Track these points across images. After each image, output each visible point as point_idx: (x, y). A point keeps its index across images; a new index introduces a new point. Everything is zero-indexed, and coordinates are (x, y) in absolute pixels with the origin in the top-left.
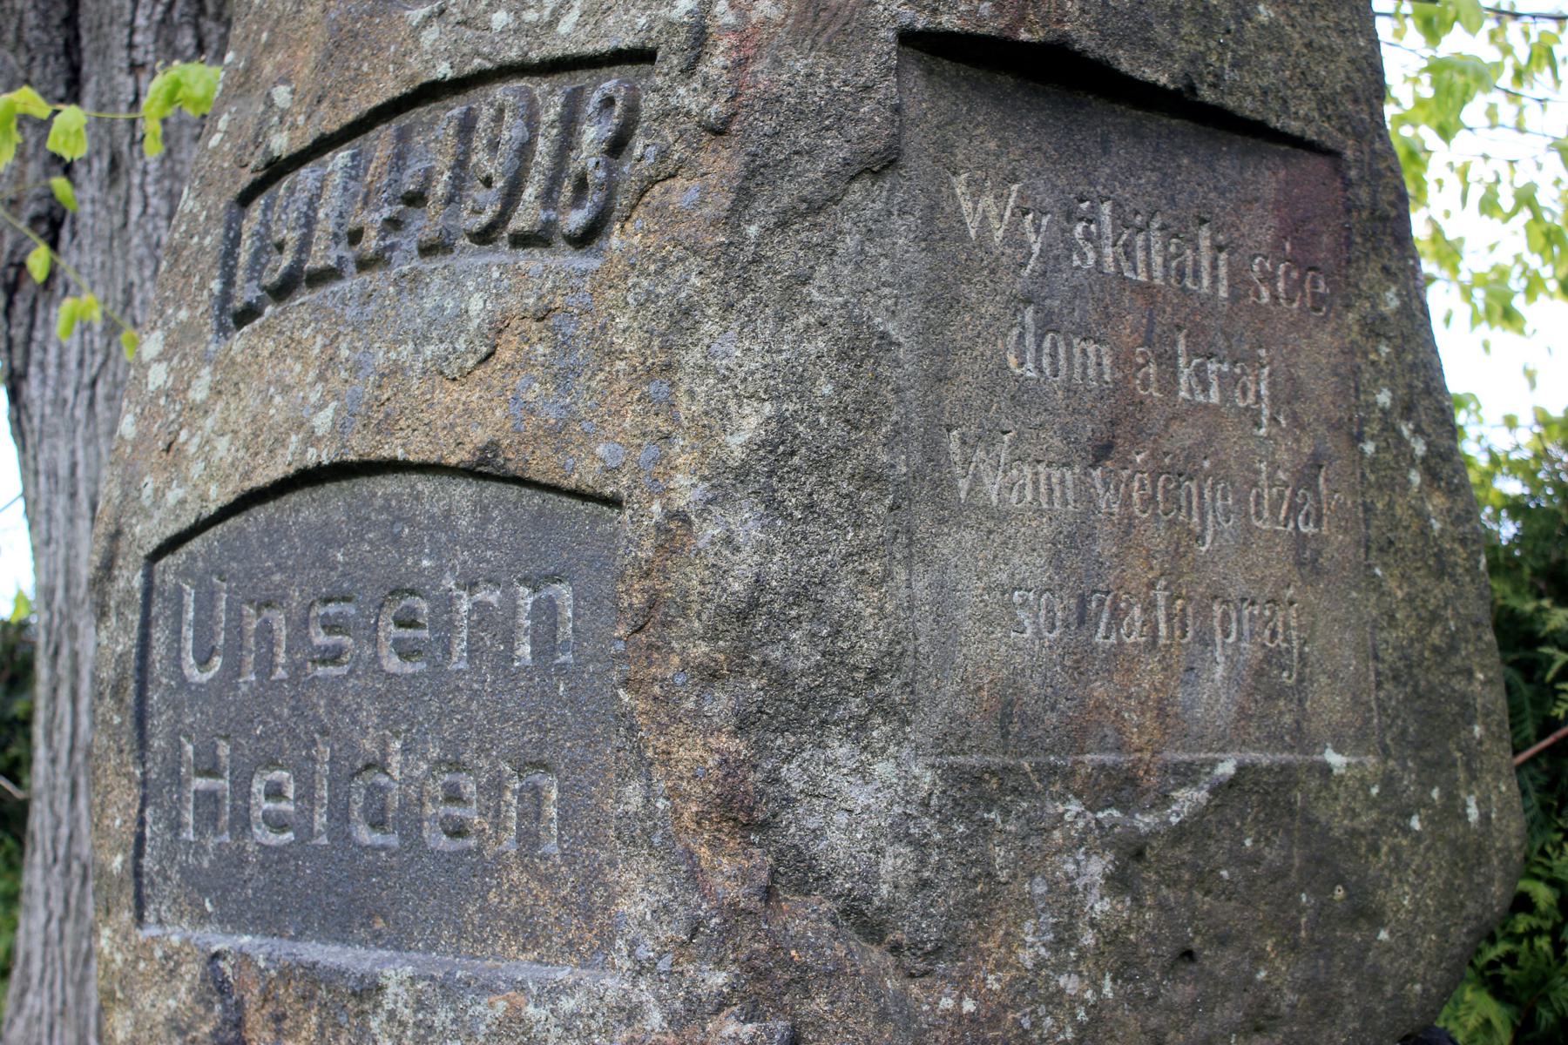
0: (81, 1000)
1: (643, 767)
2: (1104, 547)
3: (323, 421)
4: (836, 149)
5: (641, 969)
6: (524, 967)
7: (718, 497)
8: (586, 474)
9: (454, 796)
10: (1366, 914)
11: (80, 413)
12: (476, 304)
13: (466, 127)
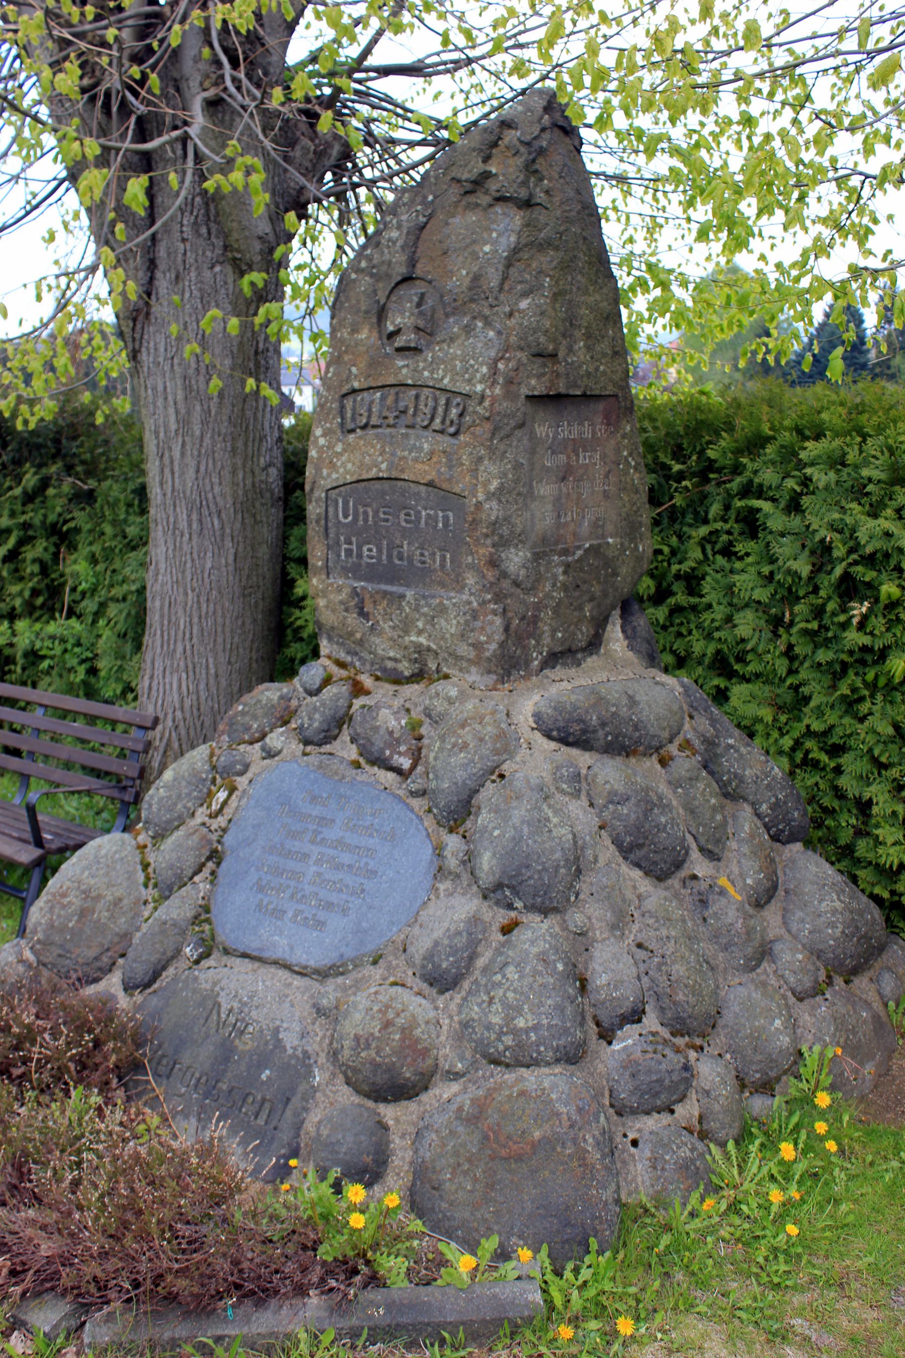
0: (184, 577)
1: (472, 554)
2: (563, 500)
3: (384, 466)
4: (513, 423)
5: (471, 594)
6: (442, 592)
7: (488, 499)
8: (457, 490)
9: (422, 555)
10: (615, 574)
11: (167, 368)
12: (426, 446)
13: (417, 397)
